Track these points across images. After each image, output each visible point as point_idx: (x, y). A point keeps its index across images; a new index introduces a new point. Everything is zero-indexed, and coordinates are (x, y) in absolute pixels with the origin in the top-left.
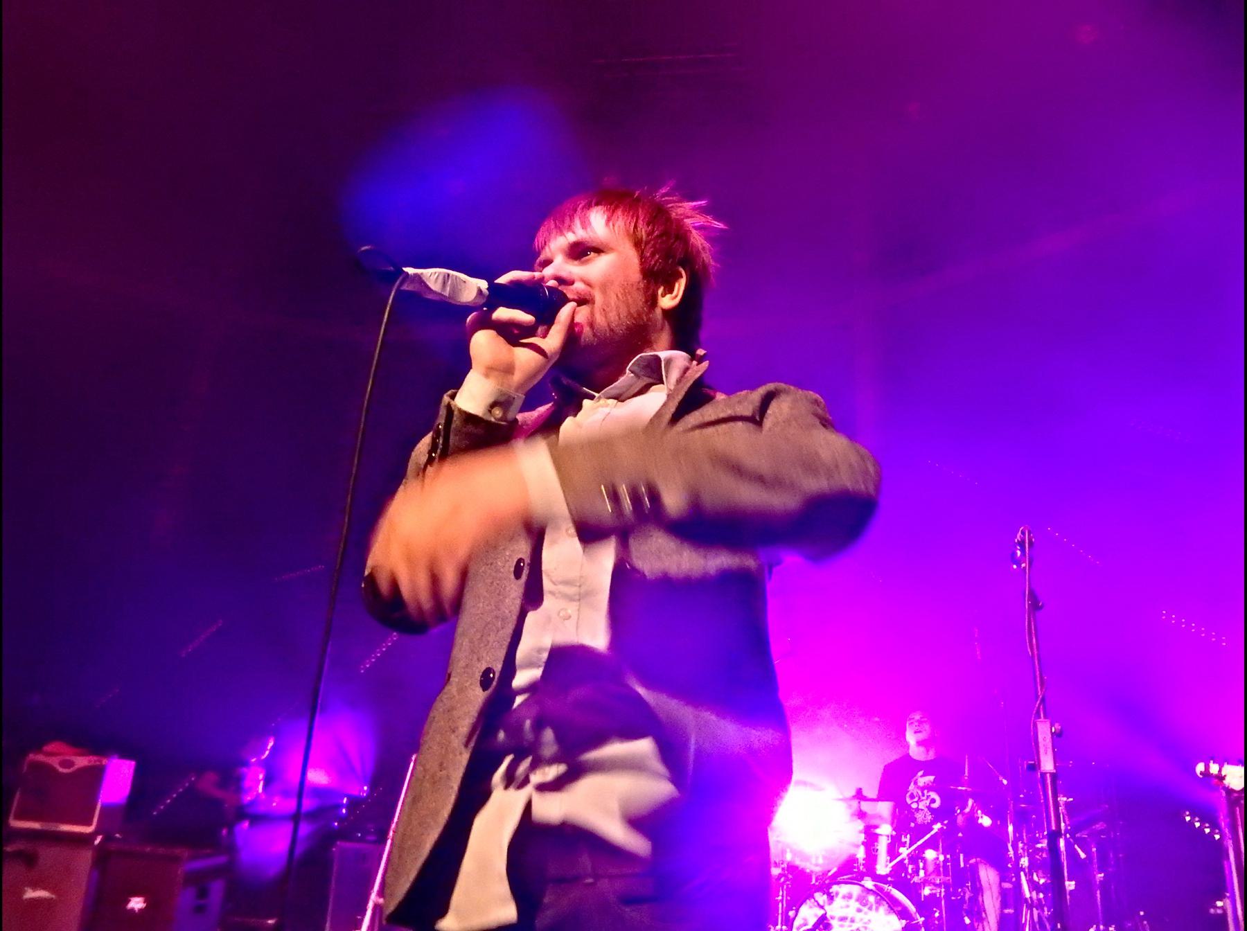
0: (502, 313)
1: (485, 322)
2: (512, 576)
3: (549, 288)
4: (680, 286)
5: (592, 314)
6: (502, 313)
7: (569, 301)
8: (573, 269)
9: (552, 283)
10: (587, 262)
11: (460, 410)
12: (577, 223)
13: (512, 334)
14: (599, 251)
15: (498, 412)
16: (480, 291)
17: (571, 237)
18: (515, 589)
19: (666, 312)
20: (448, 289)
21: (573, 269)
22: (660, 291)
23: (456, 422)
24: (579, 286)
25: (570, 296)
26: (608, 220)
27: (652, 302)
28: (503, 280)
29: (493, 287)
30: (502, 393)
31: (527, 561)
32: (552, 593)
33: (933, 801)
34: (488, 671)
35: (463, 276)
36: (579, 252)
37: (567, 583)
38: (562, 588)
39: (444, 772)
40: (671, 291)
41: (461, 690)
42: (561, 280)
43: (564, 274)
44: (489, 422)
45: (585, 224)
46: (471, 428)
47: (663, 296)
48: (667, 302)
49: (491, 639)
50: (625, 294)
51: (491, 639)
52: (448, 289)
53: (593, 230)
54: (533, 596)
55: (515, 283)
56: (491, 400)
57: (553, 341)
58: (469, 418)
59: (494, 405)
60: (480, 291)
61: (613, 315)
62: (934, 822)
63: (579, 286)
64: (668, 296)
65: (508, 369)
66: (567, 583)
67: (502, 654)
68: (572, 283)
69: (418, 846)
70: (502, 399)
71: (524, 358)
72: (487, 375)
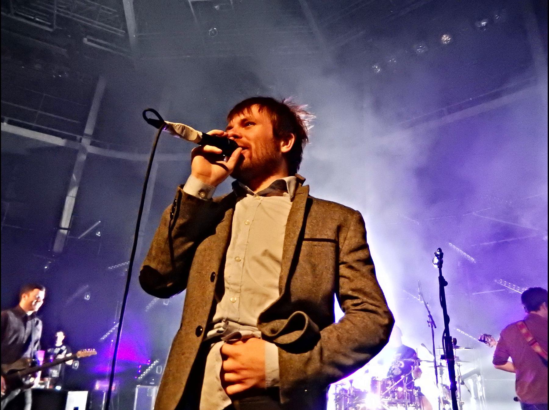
0: (208, 148)
1: (199, 152)
2: (210, 280)
3: (230, 140)
4: (292, 142)
5: (251, 153)
6: (208, 148)
7: (238, 147)
8: (241, 131)
9: (232, 138)
10: (249, 128)
11: (185, 193)
12: (246, 111)
13: (212, 158)
14: (254, 124)
15: (203, 195)
16: (198, 136)
17: (242, 117)
18: (211, 287)
19: (284, 154)
20: (184, 133)
21: (241, 131)
22: (282, 143)
23: (183, 199)
24: (244, 139)
25: (239, 144)
26: (259, 111)
27: (278, 148)
28: (210, 133)
29: (204, 135)
30: (205, 186)
31: (217, 273)
32: (228, 288)
33: (401, 365)
34: (200, 327)
35: (191, 128)
36: (245, 124)
37: (235, 284)
38: (232, 286)
39: (179, 375)
40: (287, 144)
41: (187, 334)
42: (235, 136)
43: (238, 134)
44: (199, 199)
45: (249, 111)
46: (189, 202)
47: (283, 146)
48: (285, 149)
49: (201, 310)
50: (265, 144)
51: (201, 310)
52: (184, 133)
53: (252, 115)
54: (220, 291)
55: (214, 135)
56: (199, 189)
57: (230, 163)
58: (189, 197)
59: (201, 191)
60: (198, 136)
61: (260, 154)
62: (402, 374)
63: (244, 139)
64: (286, 146)
65: (208, 175)
66: (235, 284)
67: (206, 319)
68: (241, 137)
69: (150, 399)
70: (205, 189)
71: (216, 170)
72: (198, 177)
